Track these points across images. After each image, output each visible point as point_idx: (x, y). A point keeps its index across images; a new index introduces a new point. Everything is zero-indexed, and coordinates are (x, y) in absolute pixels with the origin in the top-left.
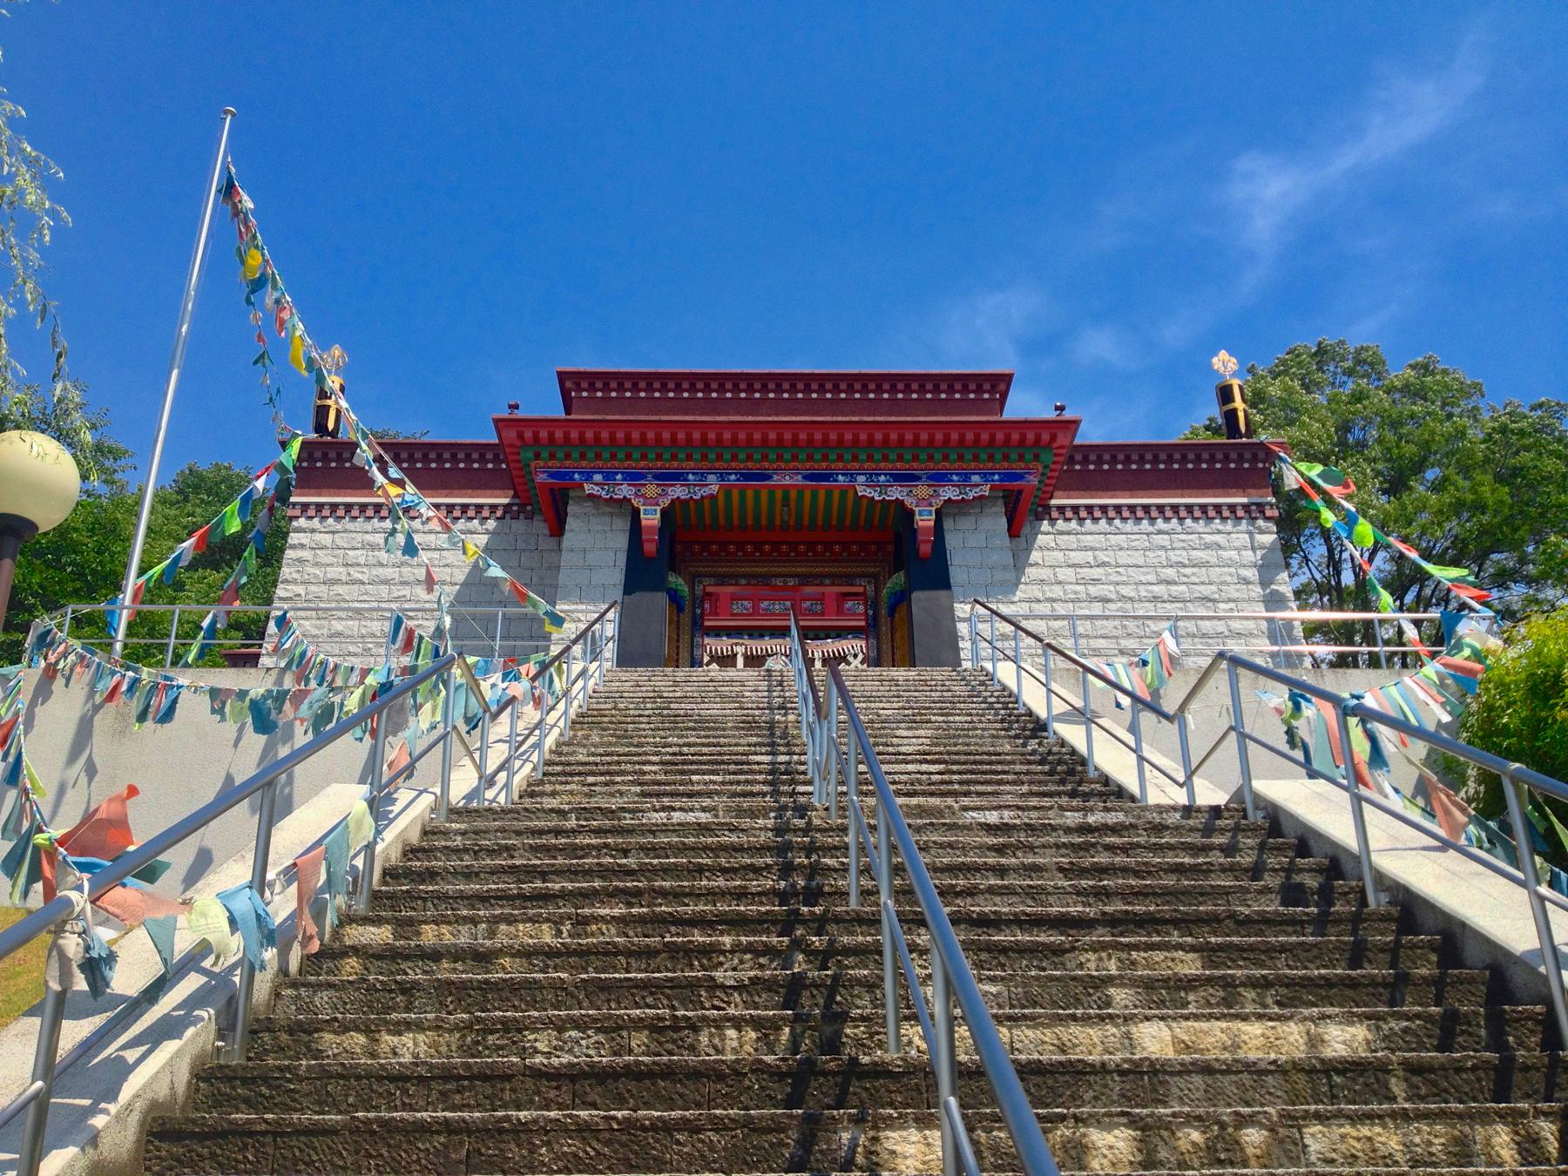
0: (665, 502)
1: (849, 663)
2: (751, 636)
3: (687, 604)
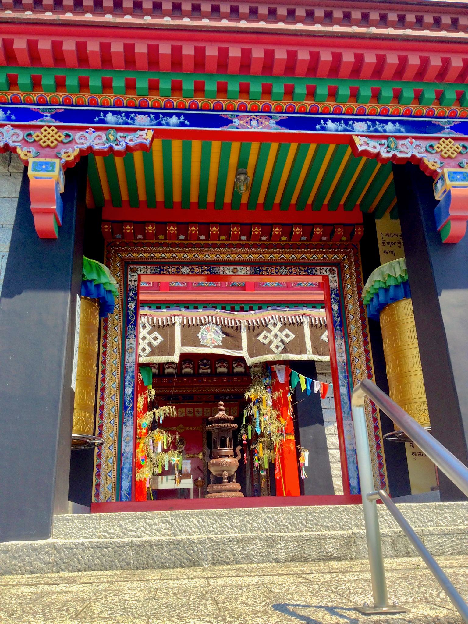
0: (71, 153)
1: (270, 331)
2: (187, 308)
3: (117, 300)
